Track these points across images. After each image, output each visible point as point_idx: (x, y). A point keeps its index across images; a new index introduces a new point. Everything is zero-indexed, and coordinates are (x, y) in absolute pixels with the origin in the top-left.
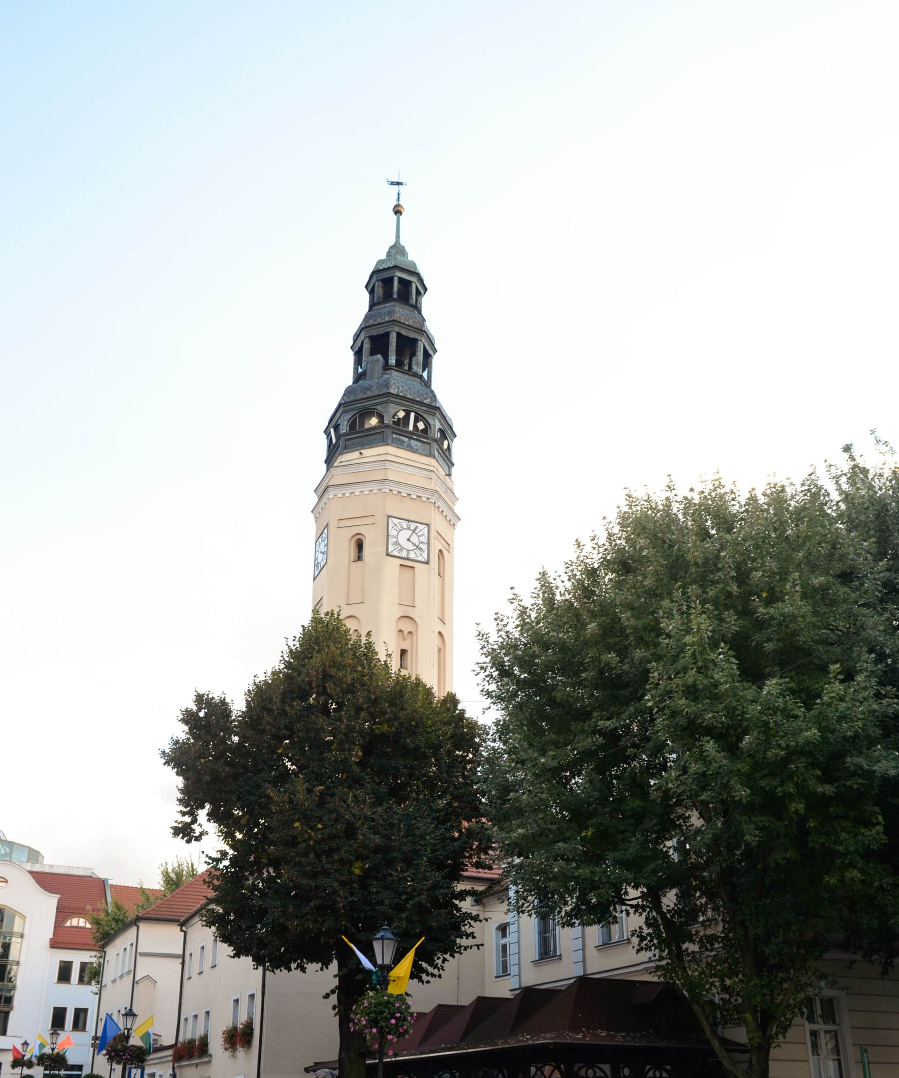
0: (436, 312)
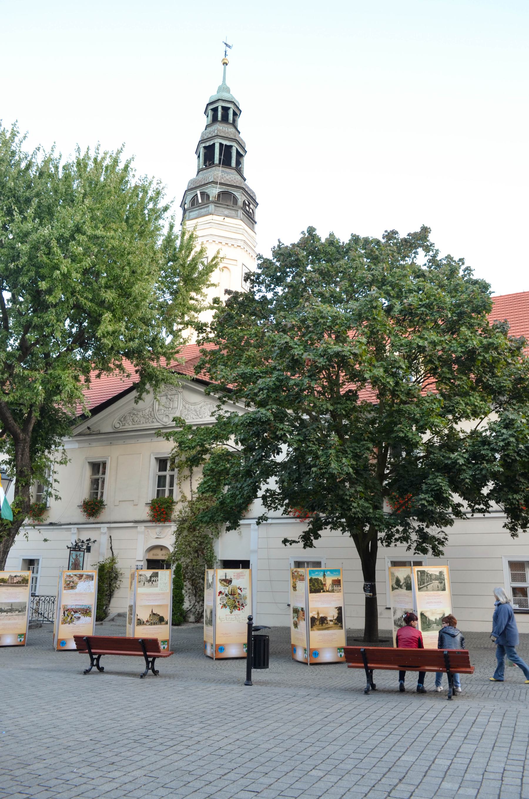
0: (248, 129)
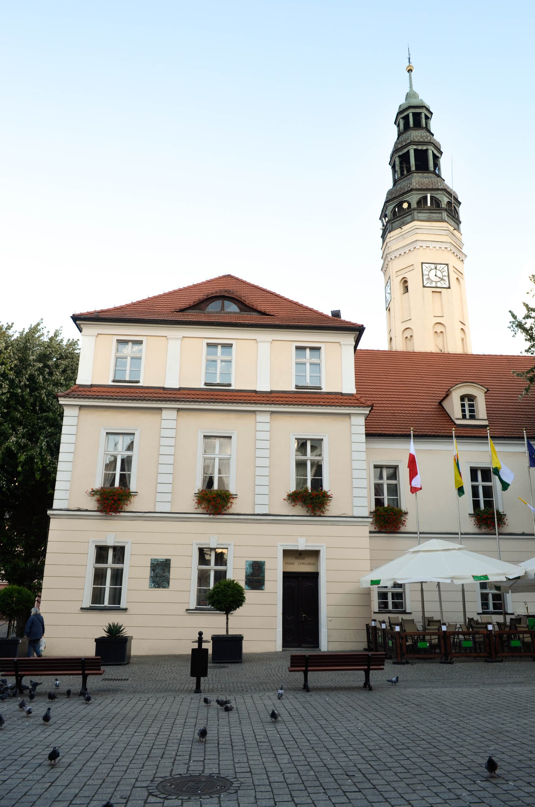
0: (441, 129)
